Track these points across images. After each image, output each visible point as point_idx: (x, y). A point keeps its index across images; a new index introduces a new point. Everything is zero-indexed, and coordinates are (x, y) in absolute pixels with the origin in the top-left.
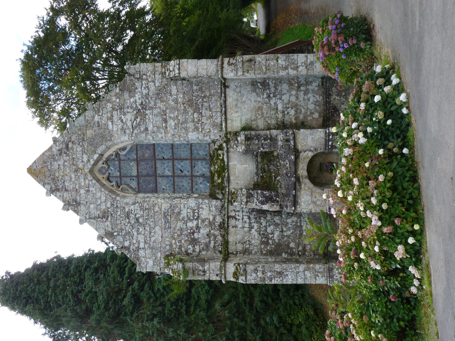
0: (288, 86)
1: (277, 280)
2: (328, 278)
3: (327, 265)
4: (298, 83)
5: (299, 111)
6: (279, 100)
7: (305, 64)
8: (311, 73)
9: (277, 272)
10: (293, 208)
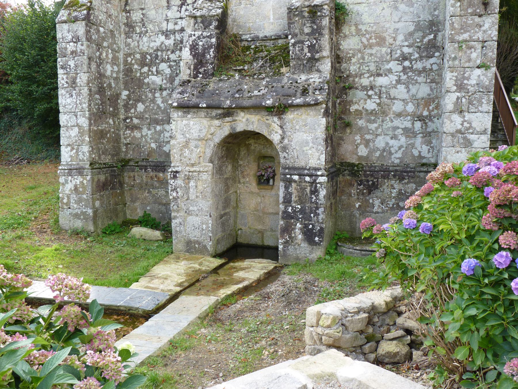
0: (425, 95)
1: (63, 79)
2: (69, 167)
3: (87, 166)
4: (430, 118)
5: (373, 118)
6: (396, 78)
7: (468, 129)
8: (447, 140)
9: (76, 78)
10: (175, 104)
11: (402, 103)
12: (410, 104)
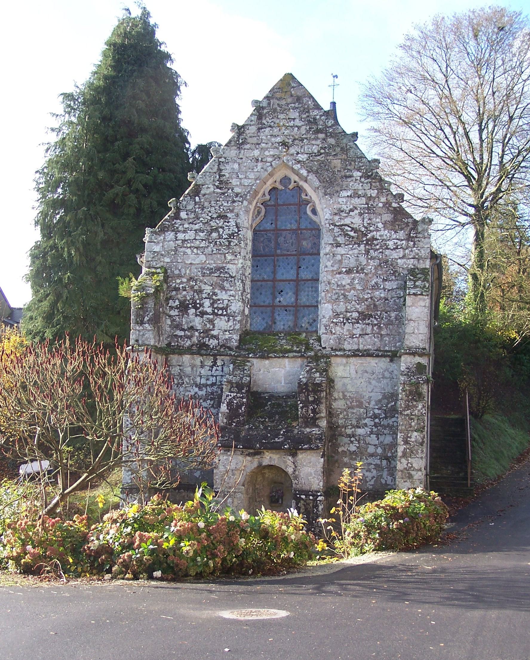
5: (354, 457)
7: (410, 468)
11: (374, 447)
12: (379, 448)
